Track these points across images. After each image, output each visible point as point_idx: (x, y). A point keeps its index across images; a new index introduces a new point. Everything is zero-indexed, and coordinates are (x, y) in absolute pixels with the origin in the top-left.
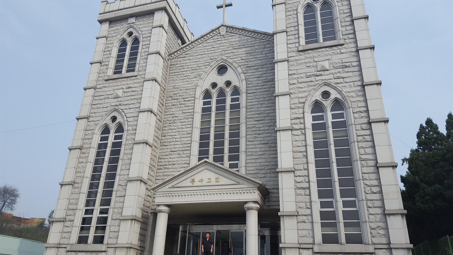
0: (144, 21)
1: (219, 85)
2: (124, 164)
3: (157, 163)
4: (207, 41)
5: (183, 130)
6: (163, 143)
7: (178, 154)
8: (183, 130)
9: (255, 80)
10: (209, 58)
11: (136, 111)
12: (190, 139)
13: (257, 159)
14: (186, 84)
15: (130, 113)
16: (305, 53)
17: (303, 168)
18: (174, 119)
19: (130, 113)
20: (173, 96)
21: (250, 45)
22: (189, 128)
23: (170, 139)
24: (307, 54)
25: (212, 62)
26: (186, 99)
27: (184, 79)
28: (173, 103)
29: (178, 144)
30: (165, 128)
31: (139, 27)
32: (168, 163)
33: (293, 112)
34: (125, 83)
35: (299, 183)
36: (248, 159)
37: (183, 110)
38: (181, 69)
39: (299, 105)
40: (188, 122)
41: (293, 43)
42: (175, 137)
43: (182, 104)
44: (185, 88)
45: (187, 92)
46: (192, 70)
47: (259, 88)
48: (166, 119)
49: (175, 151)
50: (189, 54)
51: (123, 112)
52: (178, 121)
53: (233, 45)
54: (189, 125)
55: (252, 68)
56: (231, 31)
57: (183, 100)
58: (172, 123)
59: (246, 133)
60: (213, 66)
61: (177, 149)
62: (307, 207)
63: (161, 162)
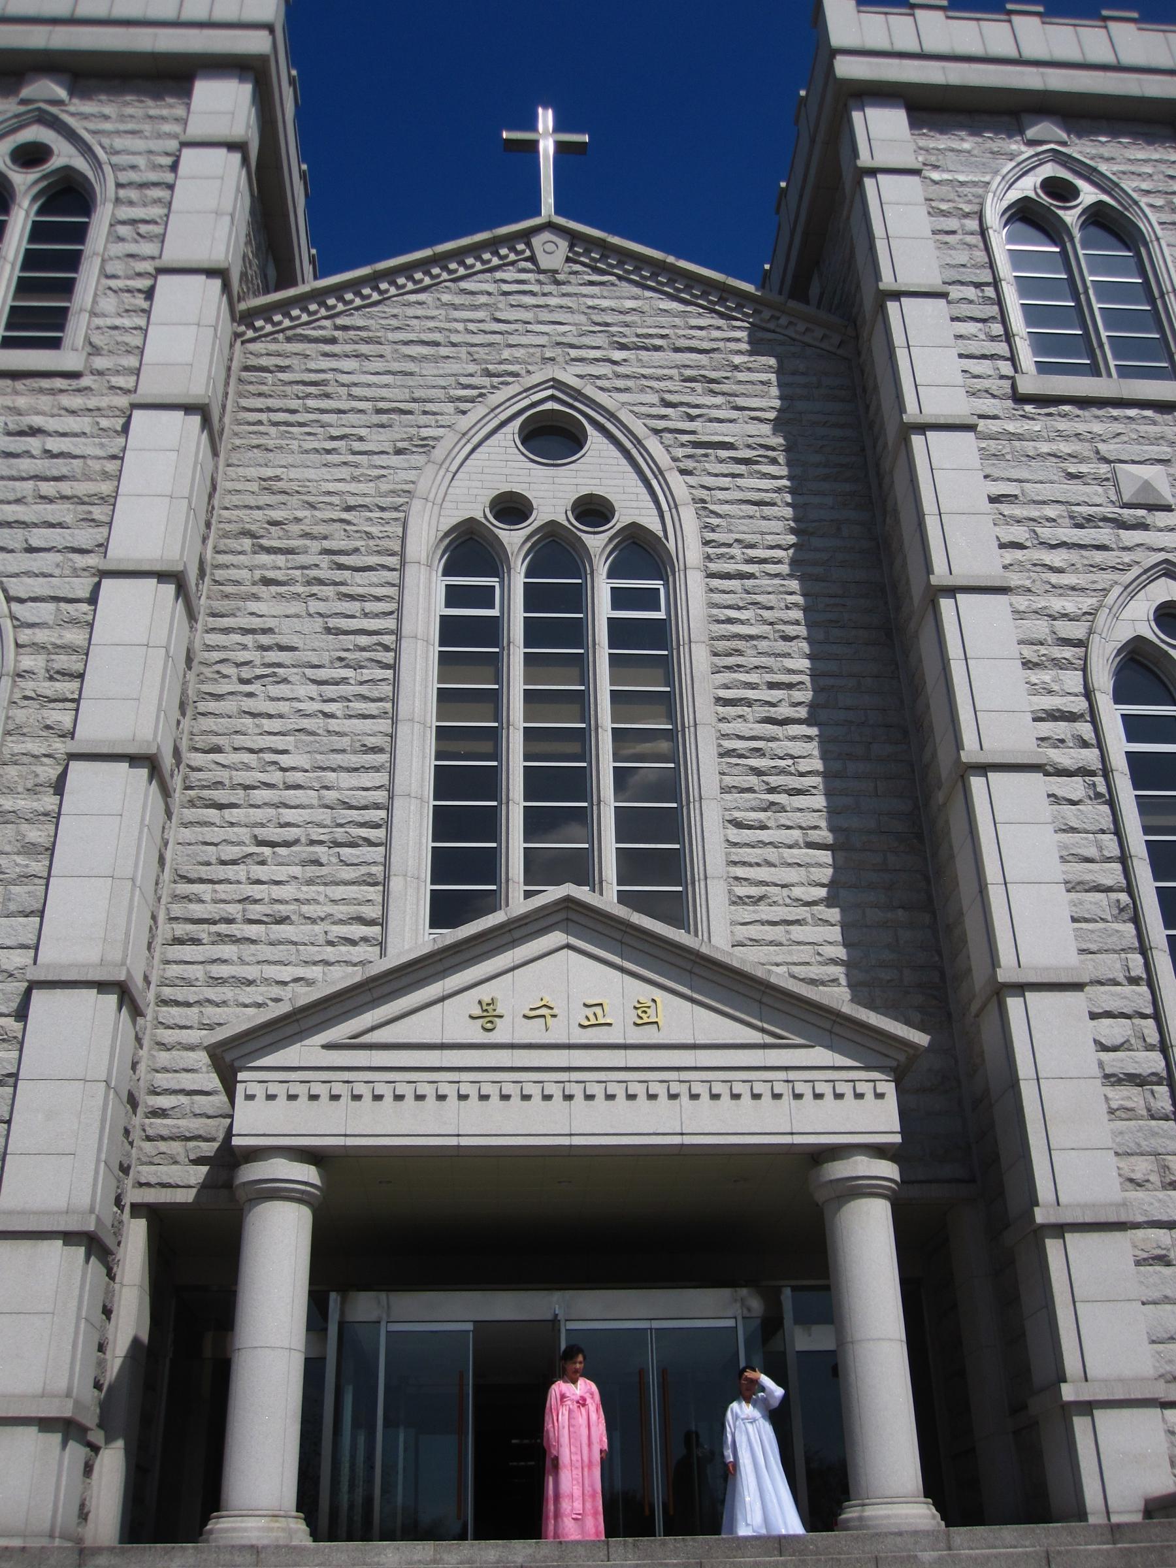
4: (463, 285)
7: (304, 863)
8: (333, 724)
9: (742, 514)
11: (75, 569)
12: (381, 778)
14: (340, 480)
17: (1121, 975)
18: (273, 656)
20: (262, 532)
23: (248, 767)
25: (493, 387)
26: (343, 559)
27: (328, 452)
28: (263, 567)
29: (305, 801)
33: (1034, 680)
35: (1115, 1049)
40: (361, 683)
41: (984, 357)
42: (285, 761)
43: (321, 582)
44: (335, 500)
45: (348, 523)
46: (379, 411)
49: (287, 844)
50: (359, 328)
52: (295, 670)
62: (1168, 1180)
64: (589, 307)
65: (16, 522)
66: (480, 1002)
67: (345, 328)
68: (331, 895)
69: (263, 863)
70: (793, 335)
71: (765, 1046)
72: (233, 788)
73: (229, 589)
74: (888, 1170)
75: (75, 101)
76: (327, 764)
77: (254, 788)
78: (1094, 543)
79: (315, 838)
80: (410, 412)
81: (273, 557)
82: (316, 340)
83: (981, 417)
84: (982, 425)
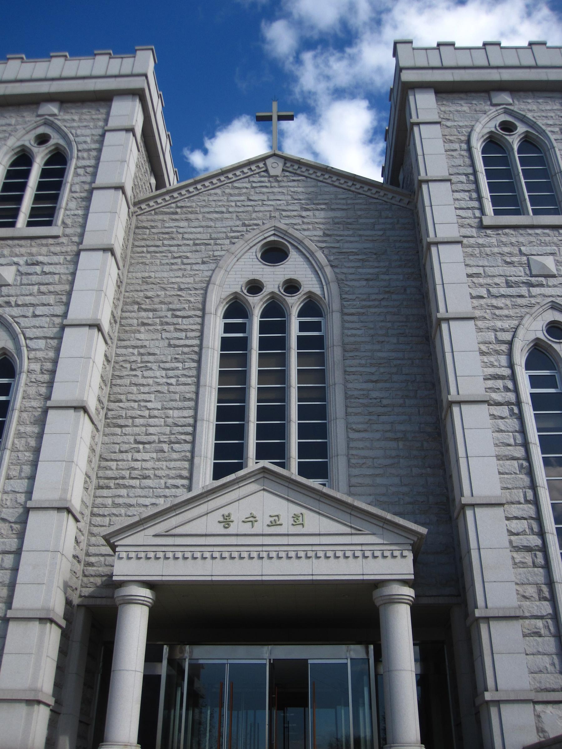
0: (82, 114)
1: (268, 286)
2: (14, 462)
3: (96, 469)
4: (236, 184)
5: (170, 390)
6: (114, 418)
7: (157, 451)
8: (172, 388)
10: (241, 223)
13: (377, 475)
14: (177, 277)
15: (34, 327)
16: (497, 232)
18: (146, 358)
19: (34, 327)
20: (143, 302)
21: (345, 207)
22: (189, 384)
23: (133, 409)
24: (503, 236)
25: (247, 231)
26: (178, 313)
27: (172, 264)
28: (142, 318)
29: (158, 423)
30: (119, 381)
31: (68, 125)
32: (128, 472)
33: (486, 360)
34: (23, 250)
35: (518, 534)
36: (355, 476)
37: (172, 339)
38: (165, 239)
39: (497, 347)
41: (468, 208)
42: (149, 405)
43: (167, 324)
44: (176, 286)
47: (371, 303)
48: (121, 358)
49: (149, 443)
50: (186, 207)
51: (17, 323)
52: (155, 364)
53: (300, 200)
54: (189, 379)
55: (351, 257)
56: (296, 170)
57: (169, 314)
58: (139, 368)
59: (346, 410)
60: (251, 240)
61: (154, 436)
63: (108, 468)
64: (292, 192)
65: (30, 304)
66: (223, 515)
67: (182, 207)
68: (168, 466)
69: (139, 452)
70: (386, 200)
71: (352, 534)
72: (126, 418)
73: (127, 328)
74: (409, 592)
75: (62, 114)
76: (168, 406)
77: (136, 418)
78: (517, 294)
79: (162, 440)
80: (210, 244)
81: (147, 313)
82: (167, 213)
83: (464, 237)
84: (465, 241)
